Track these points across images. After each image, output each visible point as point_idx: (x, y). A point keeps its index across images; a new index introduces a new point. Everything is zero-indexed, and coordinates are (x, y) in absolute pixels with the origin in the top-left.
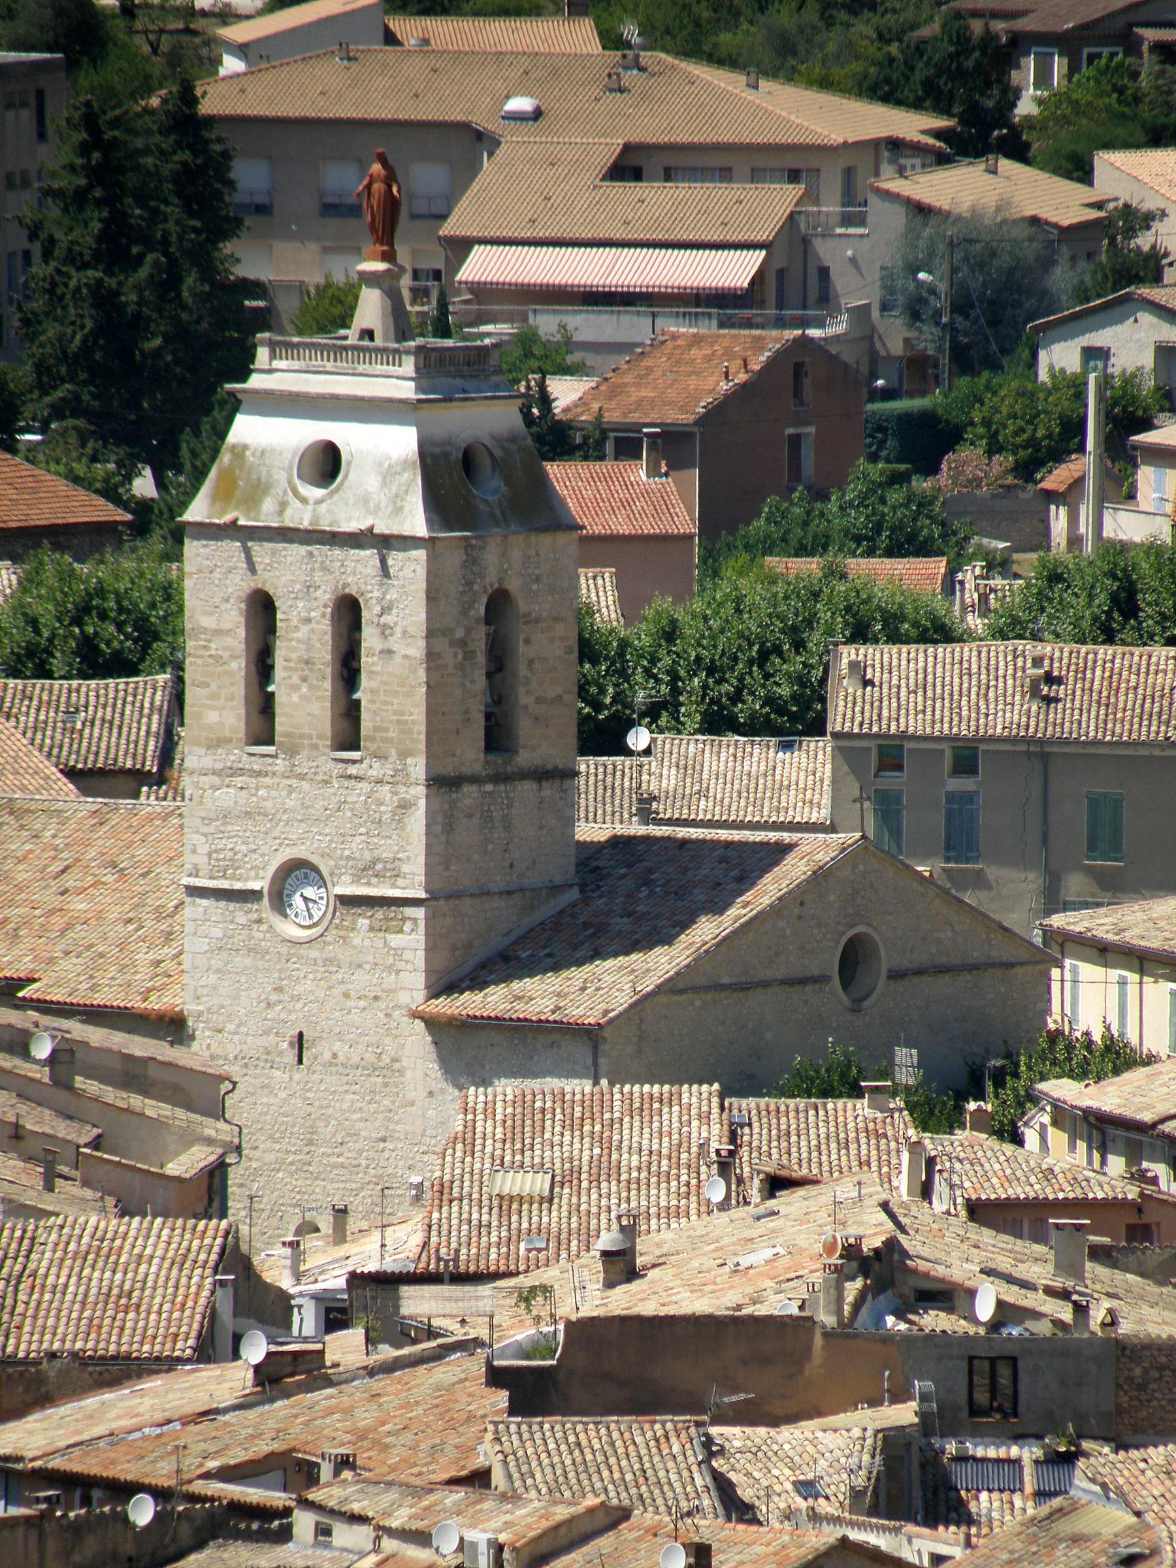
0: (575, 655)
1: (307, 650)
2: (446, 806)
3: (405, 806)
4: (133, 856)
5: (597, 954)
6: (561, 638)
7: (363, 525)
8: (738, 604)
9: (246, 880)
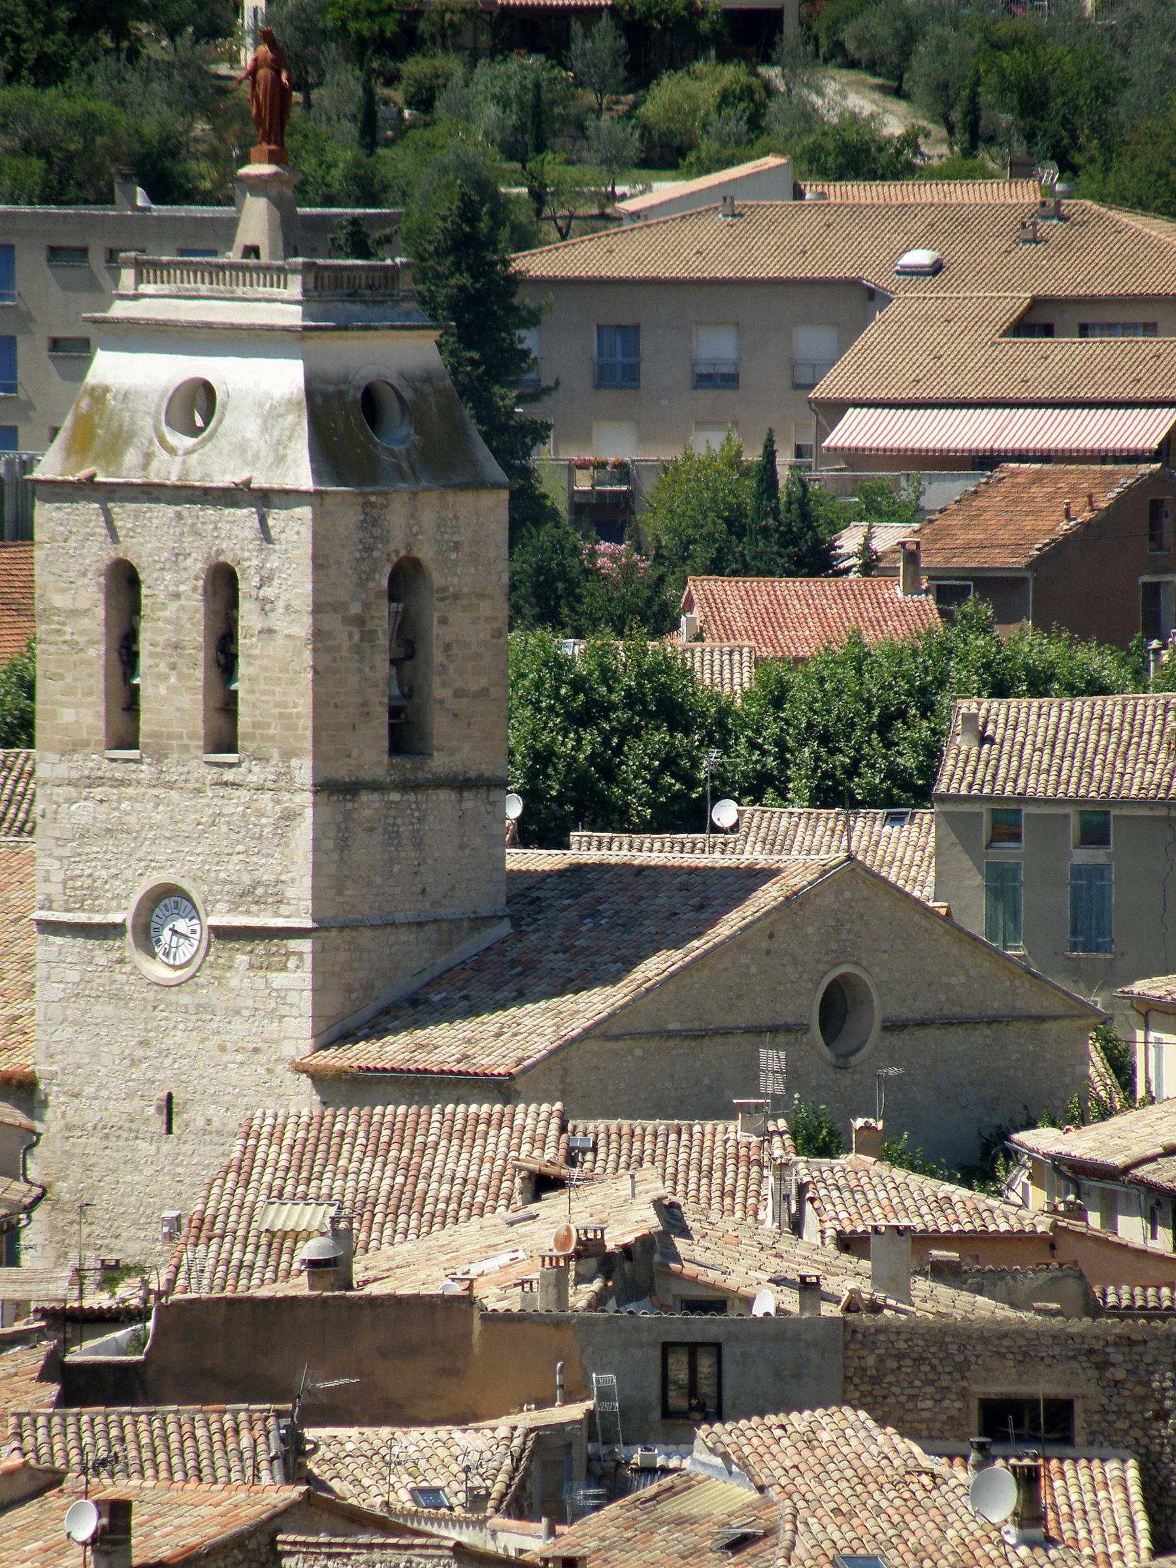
1: (176, 631)
2: (339, 818)
3: (289, 816)
4: (7, 900)
5: (521, 997)
6: (487, 619)
7: (239, 478)
8: (860, 664)
9: (107, 911)
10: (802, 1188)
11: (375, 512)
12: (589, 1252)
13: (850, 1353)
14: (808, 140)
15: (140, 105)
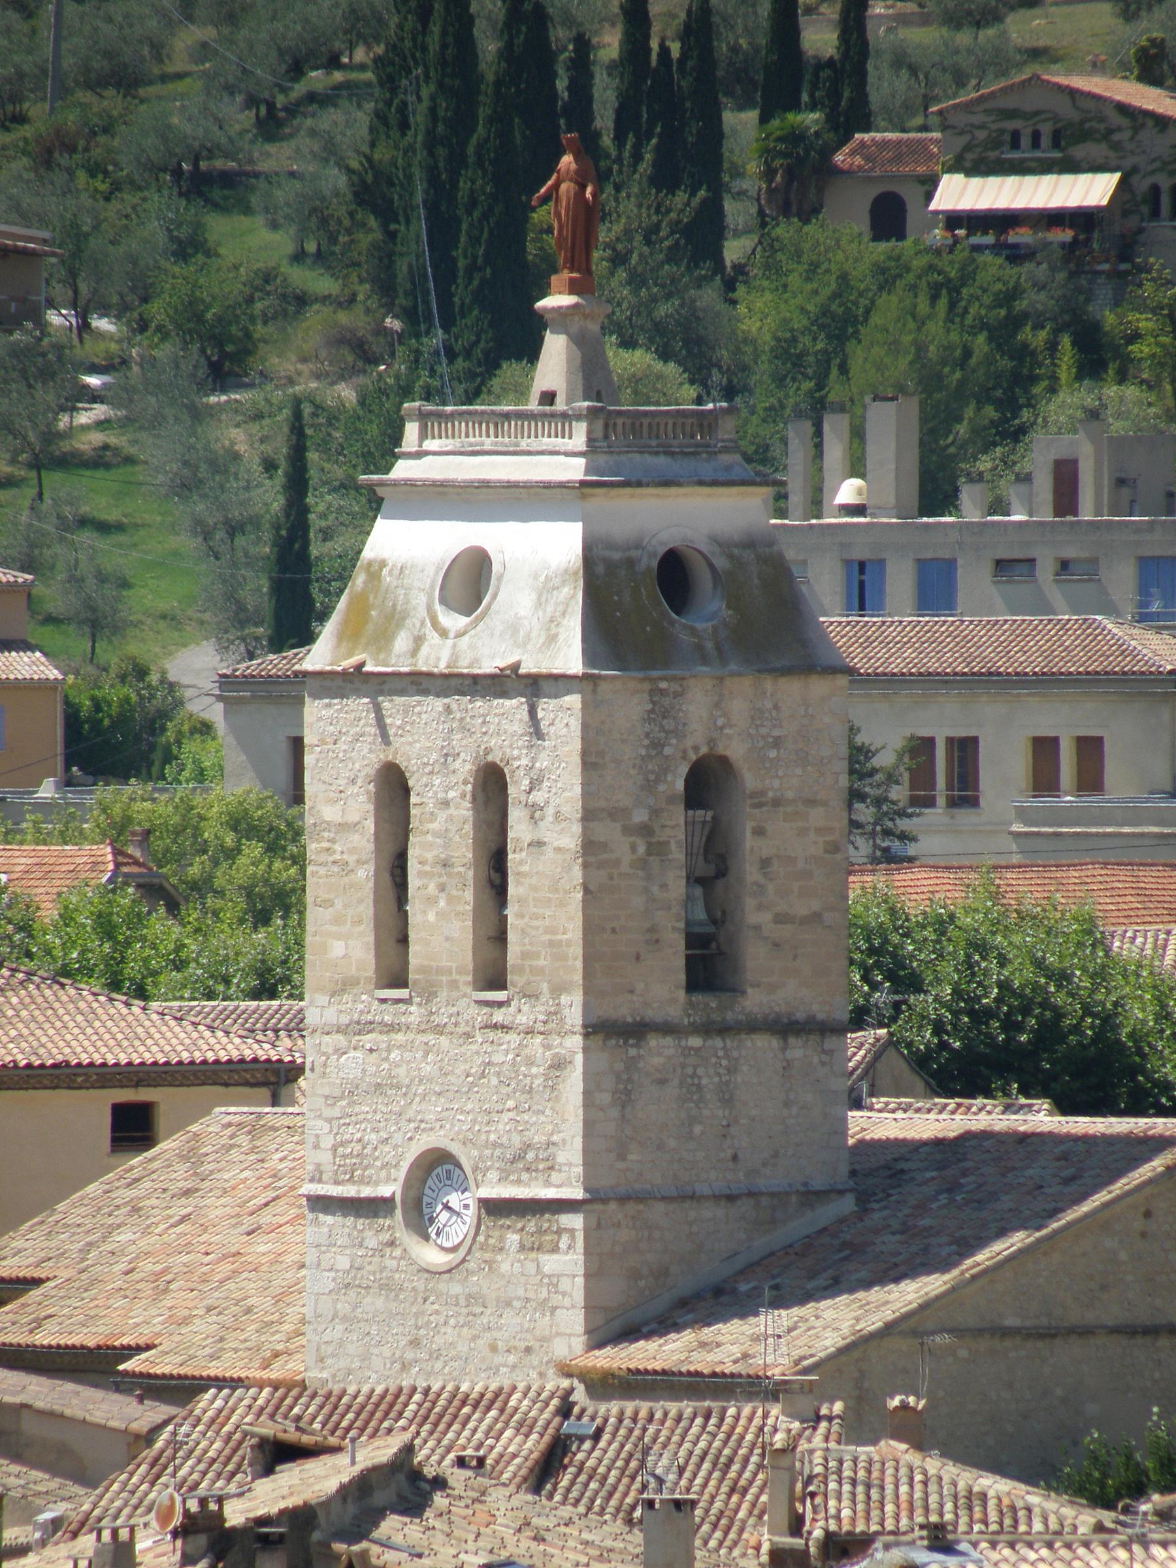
1: (446, 846)
2: (619, 1066)
3: (559, 1065)
6: (819, 831)
9: (377, 1183)
11: (666, 701)
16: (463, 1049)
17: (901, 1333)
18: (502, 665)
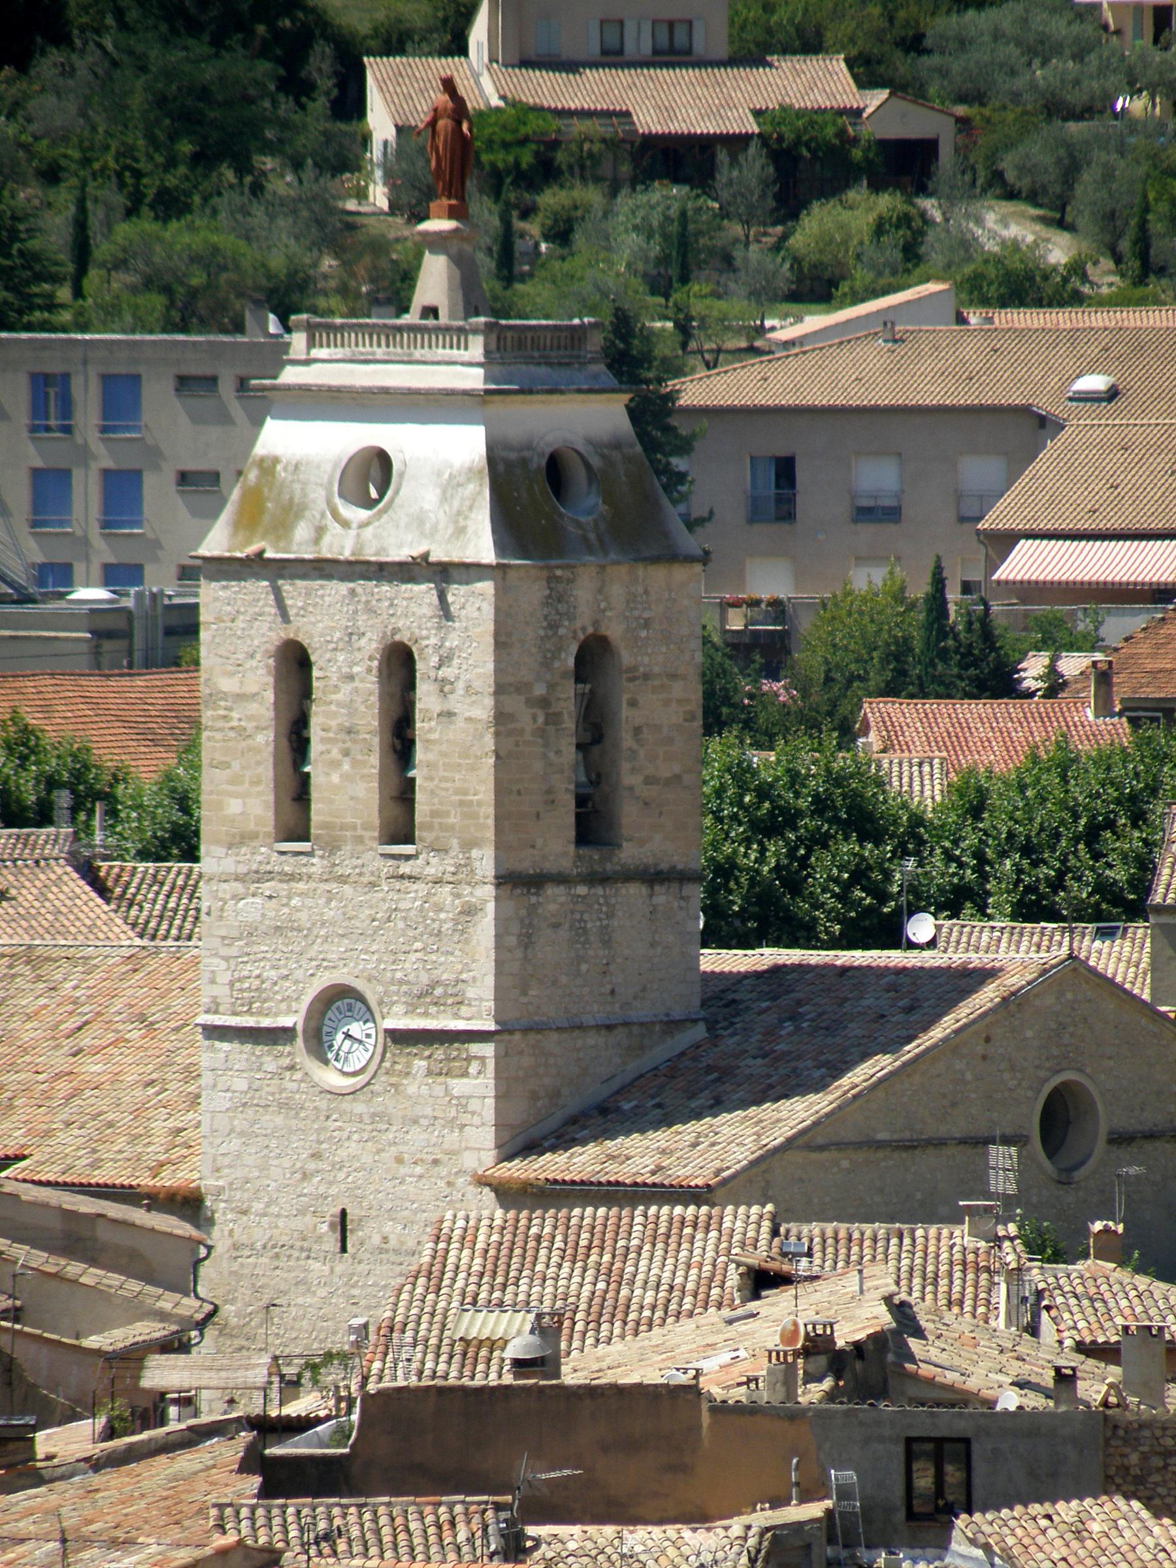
0: (699, 722)
1: (350, 715)
2: (523, 912)
3: (470, 910)
5: (717, 1106)
6: (679, 701)
9: (276, 1015)
10: (1039, 1294)
11: (560, 587)
12: (817, 1348)
13: (1112, 1450)
14: (968, 270)
15: (267, 238)
16: (368, 897)
17: (799, 1147)
18: (415, 554)
